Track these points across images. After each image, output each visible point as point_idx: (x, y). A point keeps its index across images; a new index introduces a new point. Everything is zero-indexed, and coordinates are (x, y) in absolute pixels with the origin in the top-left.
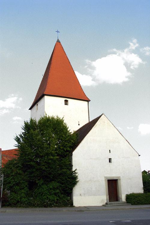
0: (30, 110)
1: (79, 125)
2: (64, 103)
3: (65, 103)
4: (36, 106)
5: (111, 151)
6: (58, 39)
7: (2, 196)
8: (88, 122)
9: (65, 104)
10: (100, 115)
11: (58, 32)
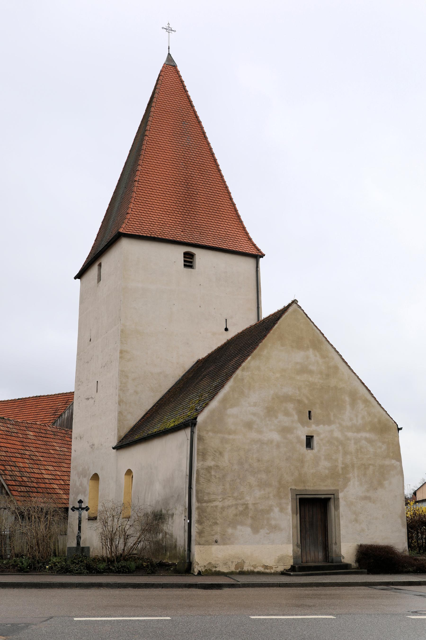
0: (78, 280)
1: (226, 329)
2: (182, 263)
3: (185, 261)
4: (94, 270)
5: (312, 414)
6: (169, 54)
7: (167, 616)
8: (253, 321)
9: (185, 266)
10: (286, 305)
11: (169, 29)
